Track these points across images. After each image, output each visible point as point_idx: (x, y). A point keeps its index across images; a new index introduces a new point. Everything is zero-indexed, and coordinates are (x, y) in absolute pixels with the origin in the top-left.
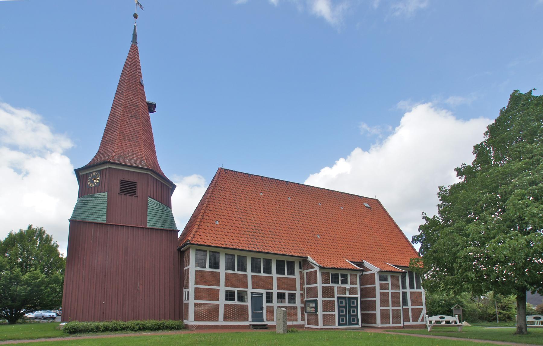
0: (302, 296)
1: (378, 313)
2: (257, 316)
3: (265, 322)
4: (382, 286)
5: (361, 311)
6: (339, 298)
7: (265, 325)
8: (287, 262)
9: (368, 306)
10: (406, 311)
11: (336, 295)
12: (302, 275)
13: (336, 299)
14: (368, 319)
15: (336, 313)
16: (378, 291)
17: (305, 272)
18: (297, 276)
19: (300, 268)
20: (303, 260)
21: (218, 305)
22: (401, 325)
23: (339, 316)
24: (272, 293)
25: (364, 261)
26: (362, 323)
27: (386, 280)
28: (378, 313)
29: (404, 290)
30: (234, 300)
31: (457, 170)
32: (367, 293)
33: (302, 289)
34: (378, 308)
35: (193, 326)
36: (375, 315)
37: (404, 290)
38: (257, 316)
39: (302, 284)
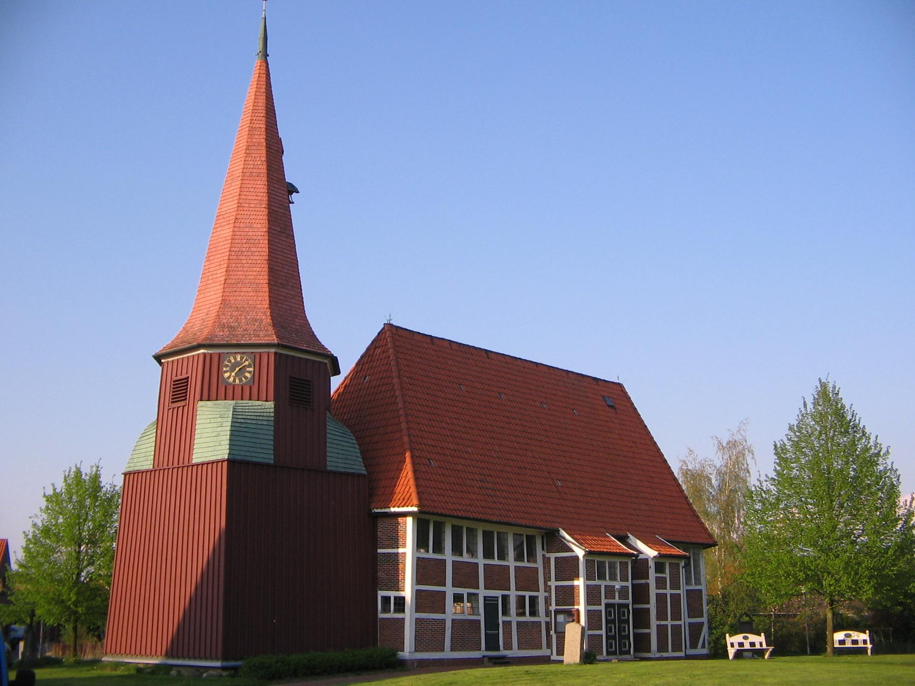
0: (547, 601)
1: (653, 632)
2: (492, 643)
3: (503, 652)
4: (660, 583)
5: (634, 628)
6: (607, 605)
7: (503, 657)
8: (527, 536)
9: (642, 618)
10: (676, 630)
11: (604, 601)
12: (546, 561)
13: (602, 608)
14: (642, 644)
15: (603, 632)
16: (653, 591)
17: (553, 556)
18: (539, 565)
19: (543, 549)
20: (546, 533)
21: (443, 621)
22: (682, 654)
23: (608, 637)
24: (508, 596)
25: (629, 535)
26: (635, 650)
27: (663, 571)
28: (653, 632)
29: (507, 619)
30: (530, 597)
31: (824, 386)
32: (640, 593)
33: (547, 589)
34: (654, 622)
35: (413, 661)
36: (649, 635)
37: (507, 619)
38: (492, 643)
39: (547, 578)
